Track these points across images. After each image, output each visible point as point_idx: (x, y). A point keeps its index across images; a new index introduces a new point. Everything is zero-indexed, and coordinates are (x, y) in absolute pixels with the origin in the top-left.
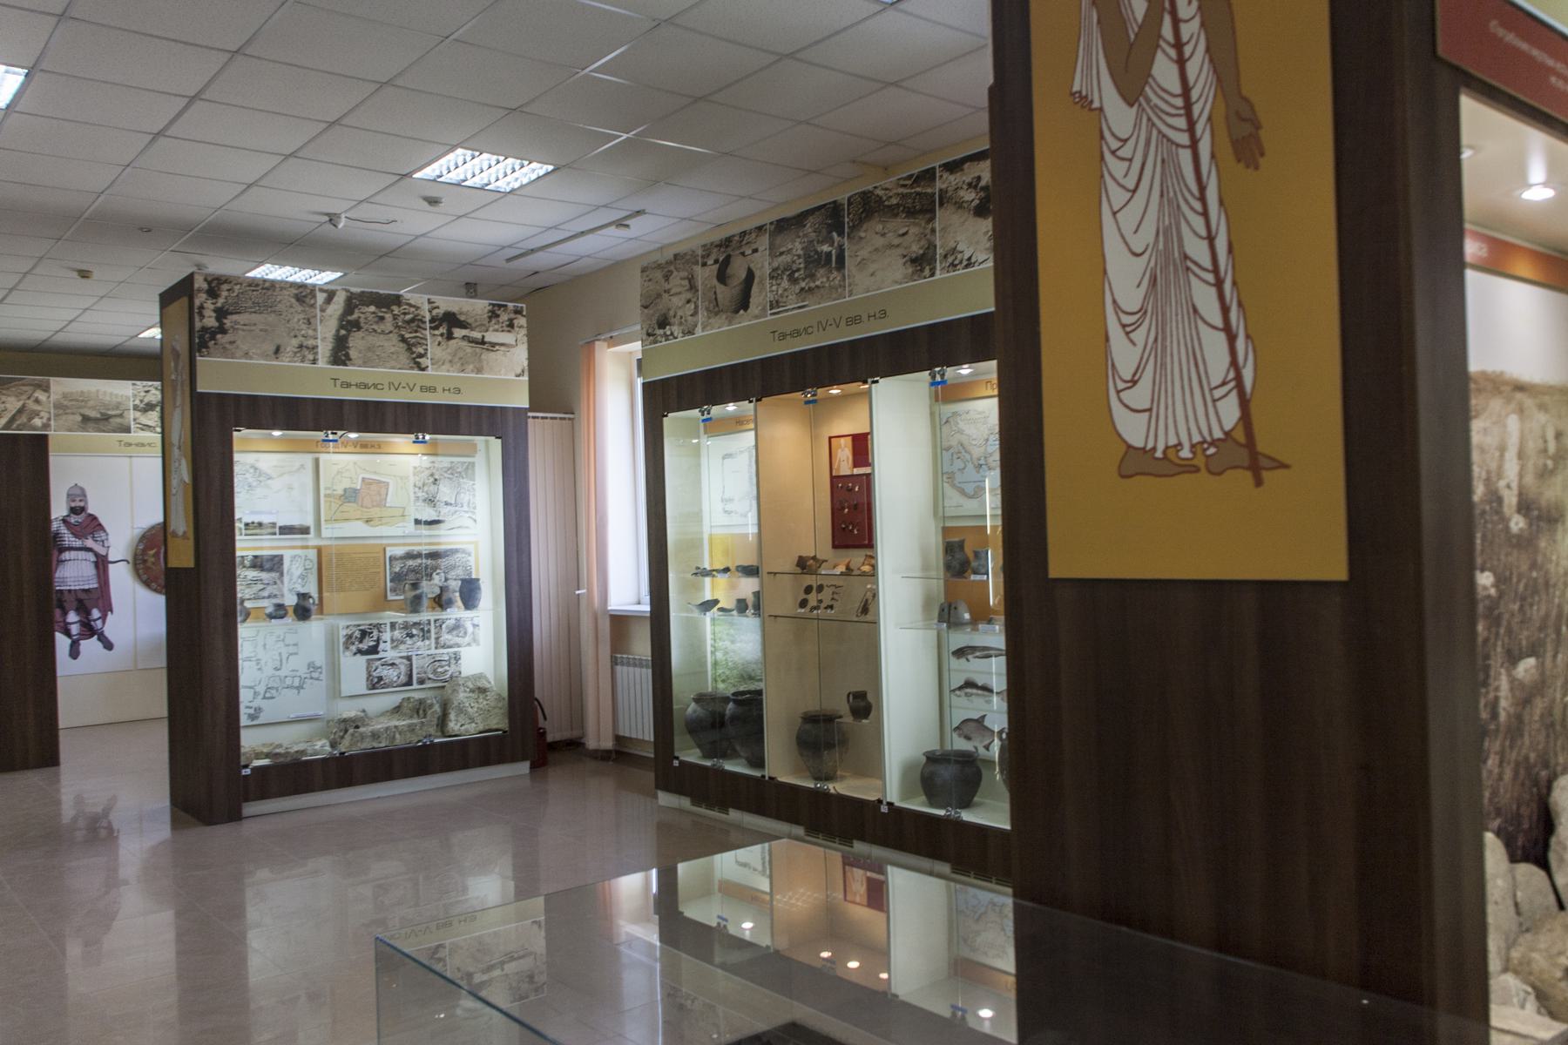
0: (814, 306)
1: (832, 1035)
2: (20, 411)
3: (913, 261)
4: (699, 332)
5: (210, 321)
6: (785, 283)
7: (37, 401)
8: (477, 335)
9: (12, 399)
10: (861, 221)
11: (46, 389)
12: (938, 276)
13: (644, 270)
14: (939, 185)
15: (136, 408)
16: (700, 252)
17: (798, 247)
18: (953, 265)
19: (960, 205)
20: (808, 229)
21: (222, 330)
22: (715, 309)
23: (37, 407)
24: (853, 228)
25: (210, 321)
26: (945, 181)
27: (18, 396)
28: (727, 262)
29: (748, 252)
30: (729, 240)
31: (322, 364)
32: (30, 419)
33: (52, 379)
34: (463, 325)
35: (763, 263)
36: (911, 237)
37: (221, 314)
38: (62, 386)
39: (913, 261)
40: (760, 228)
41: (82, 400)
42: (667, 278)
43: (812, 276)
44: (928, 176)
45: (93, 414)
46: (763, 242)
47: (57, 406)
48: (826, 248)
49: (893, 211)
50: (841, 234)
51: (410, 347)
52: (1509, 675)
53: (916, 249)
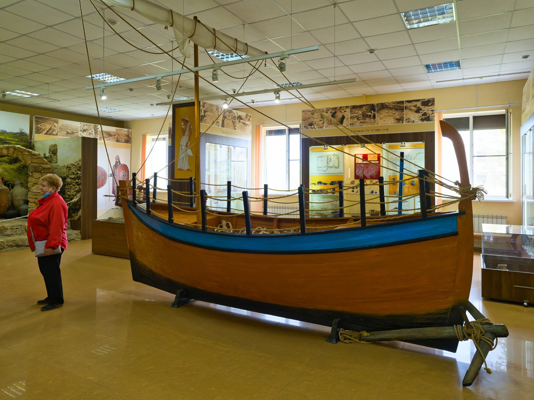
0: (365, 126)
1: (199, 287)
2: (50, 129)
3: (397, 120)
4: (324, 128)
5: (203, 114)
6: (356, 120)
7: (55, 126)
8: (244, 122)
9: (48, 125)
10: (381, 109)
11: (57, 123)
12: (404, 123)
13: (303, 111)
14: (405, 105)
15: (81, 130)
16: (325, 110)
17: (360, 112)
18: (409, 122)
19: (411, 110)
20: (364, 108)
21: (205, 116)
22: (330, 123)
23: (55, 128)
24: (378, 111)
25: (203, 114)
26: (409, 105)
27: (50, 124)
28: (335, 113)
29: (343, 111)
30: (335, 108)
31: (220, 127)
32: (53, 132)
33: (59, 120)
34: (242, 119)
35: (348, 114)
36: (397, 115)
37: (205, 112)
38: (62, 122)
39: (397, 120)
40: (347, 107)
41: (67, 127)
42: (313, 114)
43: (365, 119)
44: (402, 102)
45: (70, 132)
46: (348, 110)
47: (60, 128)
48: (369, 114)
49: (391, 108)
50: (374, 111)
51: (234, 124)
52: (55, 191)
53: (398, 117)
